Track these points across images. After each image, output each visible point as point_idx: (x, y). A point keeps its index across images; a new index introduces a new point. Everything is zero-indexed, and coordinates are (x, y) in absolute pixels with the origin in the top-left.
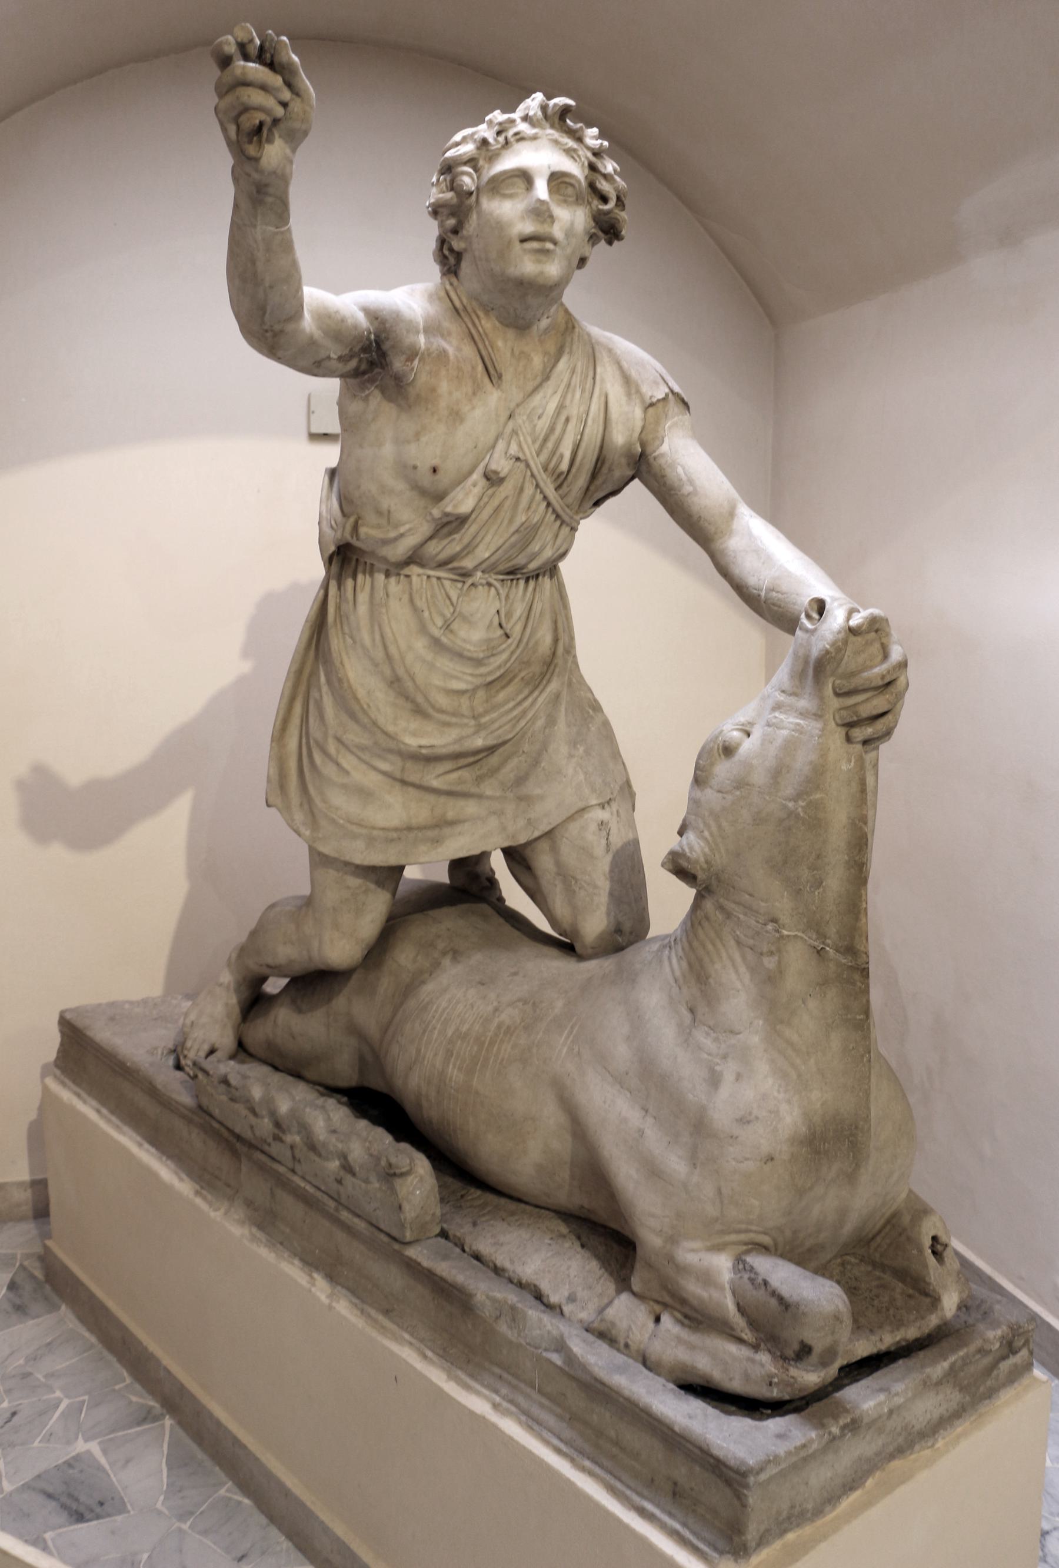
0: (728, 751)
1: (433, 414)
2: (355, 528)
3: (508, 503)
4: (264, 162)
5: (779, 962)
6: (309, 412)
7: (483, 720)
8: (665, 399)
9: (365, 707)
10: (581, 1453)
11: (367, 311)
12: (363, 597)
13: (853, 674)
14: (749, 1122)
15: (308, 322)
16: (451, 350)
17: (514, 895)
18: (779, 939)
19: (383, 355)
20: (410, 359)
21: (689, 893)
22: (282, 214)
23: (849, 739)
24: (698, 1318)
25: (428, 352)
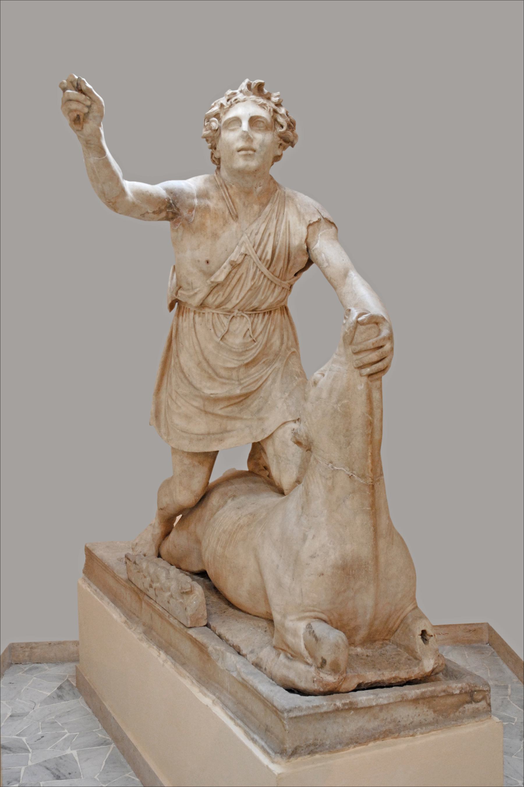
1: (204, 236)
3: (244, 276)
5: (333, 482)
7: (242, 382)
8: (319, 221)
9: (187, 376)
10: (226, 707)
14: (314, 557)
18: (333, 471)
23: (361, 375)
25: (199, 207)
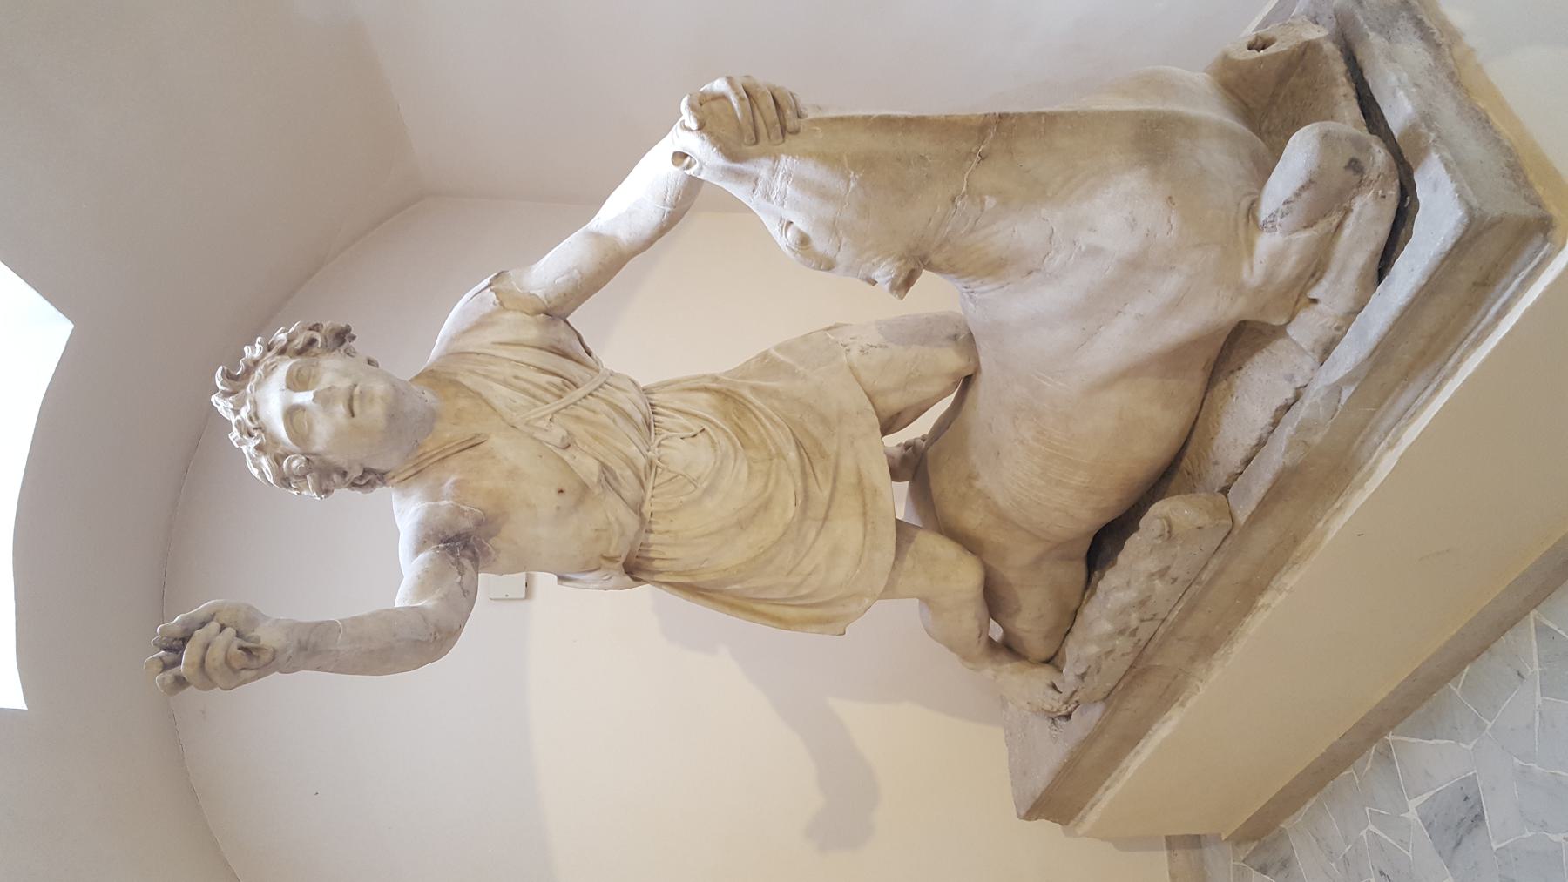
0: (804, 241)
2: (611, 559)
4: (276, 645)
6: (507, 599)
8: (497, 292)
11: (417, 552)
12: (669, 553)
13: (739, 127)
15: (427, 603)
16: (453, 479)
17: (920, 428)
19: (458, 536)
20: (462, 513)
21: (926, 276)
22: (328, 628)
23: (796, 132)
24: (1316, 267)
